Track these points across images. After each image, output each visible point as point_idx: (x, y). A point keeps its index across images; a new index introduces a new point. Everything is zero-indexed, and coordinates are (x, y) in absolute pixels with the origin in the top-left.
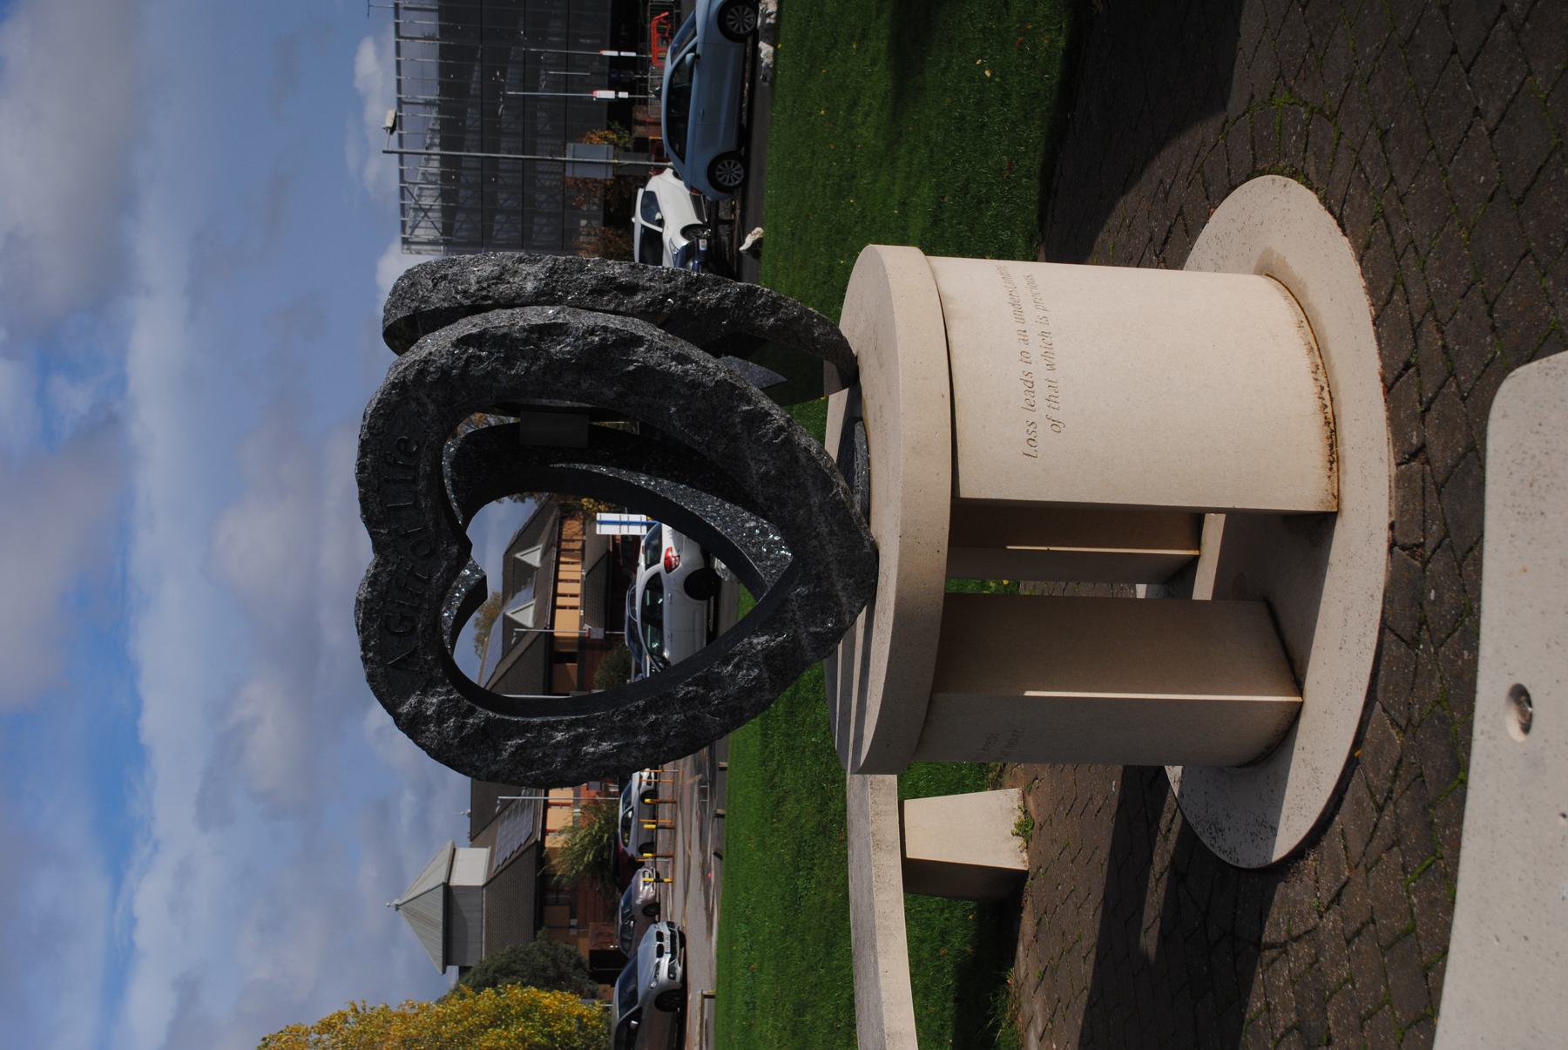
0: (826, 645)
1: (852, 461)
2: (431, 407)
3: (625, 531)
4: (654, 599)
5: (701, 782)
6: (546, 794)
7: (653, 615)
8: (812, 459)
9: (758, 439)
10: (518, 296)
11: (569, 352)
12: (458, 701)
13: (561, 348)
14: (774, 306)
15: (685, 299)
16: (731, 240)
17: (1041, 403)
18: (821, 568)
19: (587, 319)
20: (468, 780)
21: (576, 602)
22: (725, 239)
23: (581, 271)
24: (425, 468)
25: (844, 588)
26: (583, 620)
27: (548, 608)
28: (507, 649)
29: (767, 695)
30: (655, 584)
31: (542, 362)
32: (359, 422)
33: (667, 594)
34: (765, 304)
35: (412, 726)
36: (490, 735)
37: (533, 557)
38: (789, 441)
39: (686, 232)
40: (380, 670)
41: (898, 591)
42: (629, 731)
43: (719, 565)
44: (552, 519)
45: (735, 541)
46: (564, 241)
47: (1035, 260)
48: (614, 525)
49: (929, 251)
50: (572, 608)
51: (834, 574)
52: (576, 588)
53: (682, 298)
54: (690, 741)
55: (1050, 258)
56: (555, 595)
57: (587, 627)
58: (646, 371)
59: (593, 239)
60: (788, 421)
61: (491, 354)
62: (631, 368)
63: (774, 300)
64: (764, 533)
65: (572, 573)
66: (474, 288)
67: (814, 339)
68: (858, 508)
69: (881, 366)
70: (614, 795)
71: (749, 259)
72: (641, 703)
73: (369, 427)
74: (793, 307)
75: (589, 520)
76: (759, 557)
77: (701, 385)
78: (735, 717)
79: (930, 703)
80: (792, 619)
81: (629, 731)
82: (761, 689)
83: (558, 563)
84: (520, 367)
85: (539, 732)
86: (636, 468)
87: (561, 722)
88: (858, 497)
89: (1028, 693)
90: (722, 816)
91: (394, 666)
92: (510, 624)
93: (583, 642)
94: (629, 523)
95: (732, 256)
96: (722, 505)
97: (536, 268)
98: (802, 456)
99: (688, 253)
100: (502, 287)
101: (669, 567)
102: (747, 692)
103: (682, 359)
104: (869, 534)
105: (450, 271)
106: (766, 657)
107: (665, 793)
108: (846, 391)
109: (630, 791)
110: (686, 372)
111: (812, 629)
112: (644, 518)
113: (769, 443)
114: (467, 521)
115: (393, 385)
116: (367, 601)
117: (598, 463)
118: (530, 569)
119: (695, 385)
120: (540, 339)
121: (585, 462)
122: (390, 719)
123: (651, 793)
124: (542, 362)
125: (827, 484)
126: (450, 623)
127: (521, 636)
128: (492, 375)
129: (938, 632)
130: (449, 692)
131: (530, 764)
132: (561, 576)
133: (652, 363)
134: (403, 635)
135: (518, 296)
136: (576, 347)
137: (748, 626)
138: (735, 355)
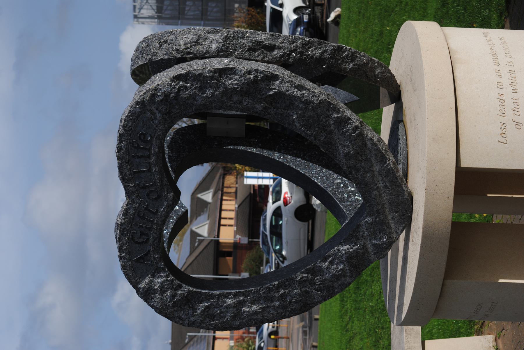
0: (382, 251)
1: (397, 145)
2: (158, 115)
3: (261, 182)
4: (277, 221)
5: (304, 327)
6: (214, 333)
7: (276, 230)
8: (374, 144)
9: (343, 134)
10: (208, 52)
11: (236, 84)
12: (172, 281)
13: (232, 82)
14: (353, 57)
15: (302, 53)
16: (322, 17)
17: (509, 112)
18: (380, 207)
19: (247, 65)
20: (170, 322)
21: (232, 222)
22: (319, 14)
23: (243, 37)
24: (155, 149)
25: (393, 219)
26: (236, 233)
27: (217, 225)
28: (193, 249)
29: (348, 280)
30: (277, 213)
31: (221, 90)
32: (118, 123)
33: (285, 218)
34: (347, 55)
35: (146, 295)
36: (190, 300)
37: (208, 196)
38: (361, 134)
39: (296, 10)
40: (129, 263)
41: (425, 220)
42: (270, 299)
43: (315, 202)
44: (218, 175)
45: (329, 191)
46: (226, 20)
47: (503, 28)
48: (255, 178)
49: (442, 24)
50: (230, 226)
51: (387, 210)
52: (232, 215)
53: (300, 52)
54: (303, 306)
55: (513, 27)
56: (220, 218)
57: (238, 237)
58: (280, 94)
59: (242, 15)
60: (361, 123)
61: (192, 85)
62: (271, 93)
63: (353, 54)
64: (346, 186)
65: (230, 206)
66: (183, 47)
67: (375, 75)
68: (401, 173)
69: (415, 91)
70: (253, 333)
71: (332, 26)
72: (276, 283)
73: (124, 127)
74: (364, 57)
75: (240, 175)
76: (343, 200)
77: (311, 102)
78: (328, 292)
79: (443, 285)
80: (363, 236)
81: (270, 299)
82: (344, 276)
83: (222, 200)
84: (209, 92)
85: (218, 299)
86: (272, 149)
87: (230, 293)
88: (400, 166)
89: (501, 281)
90: (315, 347)
91: (137, 261)
92: (194, 235)
93: (236, 245)
94: (263, 178)
95: (323, 25)
96: (321, 170)
97: (217, 36)
98: (369, 143)
99: (298, 23)
100: (198, 47)
101: (286, 203)
102: (337, 277)
103: (300, 88)
104: (407, 187)
105: (169, 38)
106: (347, 258)
107: (282, 333)
108: (393, 105)
109: (262, 331)
110: (302, 95)
111: (374, 242)
112: (271, 175)
113: (350, 136)
114: (177, 178)
115: (137, 103)
116: (122, 224)
117: (251, 146)
118: (205, 204)
119: (308, 103)
120: (220, 76)
121: (243, 145)
122: (135, 291)
123: (275, 333)
124: (221, 90)
125: (383, 159)
126: (167, 236)
127: (201, 241)
128: (193, 97)
129: (448, 244)
130: (167, 276)
131: (213, 317)
132: (224, 207)
133: (283, 90)
134: (141, 244)
135: (208, 52)
136: (240, 81)
137: (336, 240)
138: (329, 85)
